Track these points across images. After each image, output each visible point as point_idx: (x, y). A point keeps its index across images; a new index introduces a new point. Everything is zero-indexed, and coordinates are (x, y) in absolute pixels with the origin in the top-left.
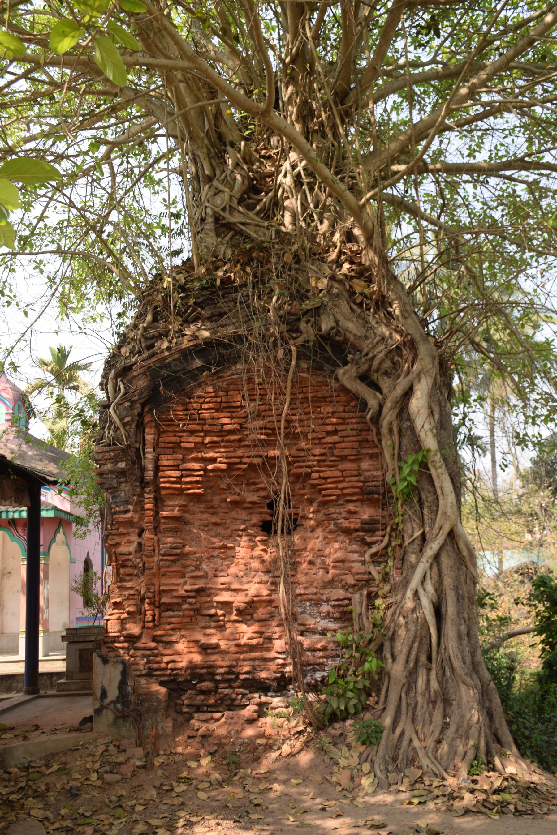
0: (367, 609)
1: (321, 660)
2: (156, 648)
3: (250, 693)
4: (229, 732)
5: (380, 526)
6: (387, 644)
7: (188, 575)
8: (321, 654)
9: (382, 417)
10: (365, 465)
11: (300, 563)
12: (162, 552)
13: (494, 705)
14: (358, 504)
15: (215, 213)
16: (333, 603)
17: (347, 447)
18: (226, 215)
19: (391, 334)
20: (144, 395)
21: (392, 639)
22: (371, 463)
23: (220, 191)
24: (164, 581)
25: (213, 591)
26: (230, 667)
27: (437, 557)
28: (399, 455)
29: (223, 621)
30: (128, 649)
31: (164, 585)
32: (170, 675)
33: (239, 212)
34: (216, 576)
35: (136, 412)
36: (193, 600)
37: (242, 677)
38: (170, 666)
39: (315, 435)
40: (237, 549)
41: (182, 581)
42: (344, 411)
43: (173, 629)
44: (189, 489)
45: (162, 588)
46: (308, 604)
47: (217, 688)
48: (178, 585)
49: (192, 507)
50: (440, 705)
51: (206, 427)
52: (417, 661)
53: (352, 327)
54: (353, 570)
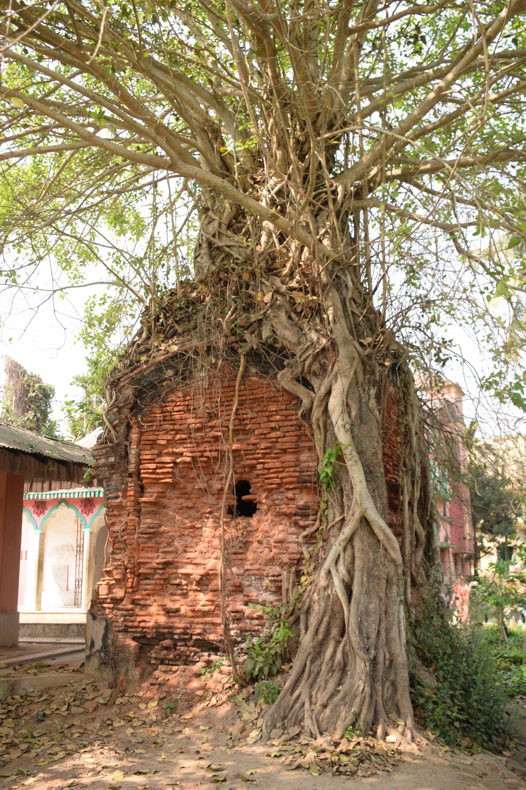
0: (294, 586)
1: (257, 628)
3: (202, 651)
4: (178, 683)
5: (310, 511)
6: (303, 617)
7: (160, 550)
8: (257, 622)
10: (304, 457)
11: (252, 542)
13: (399, 679)
14: (297, 491)
16: (271, 578)
17: (287, 442)
19: (318, 339)
21: (308, 612)
22: (309, 454)
24: (142, 555)
25: (179, 564)
26: (185, 628)
27: (350, 540)
29: (186, 589)
30: (113, 609)
32: (141, 632)
34: (185, 551)
36: (161, 571)
37: (194, 637)
38: (142, 624)
39: (261, 431)
40: (204, 529)
42: (286, 409)
43: (148, 595)
44: (163, 479)
46: (253, 578)
47: (175, 645)
48: (152, 558)
49: (168, 493)
50: (337, 675)
51: (176, 427)
53: (287, 335)
54: (290, 550)
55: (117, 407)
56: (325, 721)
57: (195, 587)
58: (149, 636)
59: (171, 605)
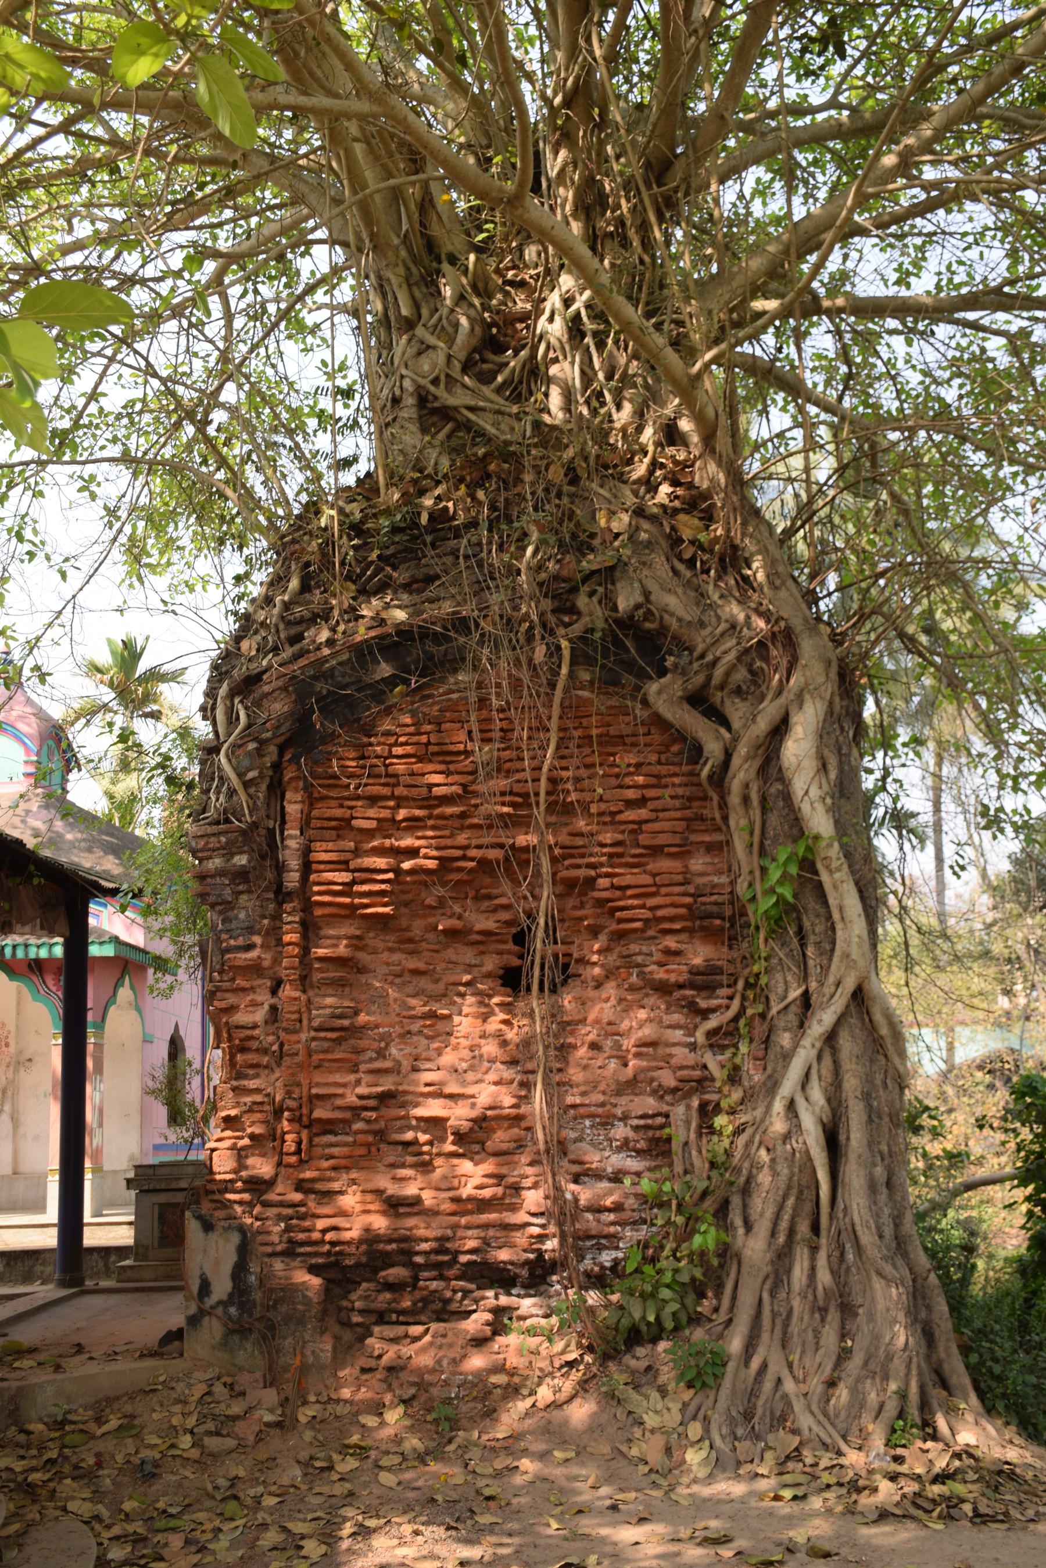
0: (700, 1135)
1: (612, 1229)
2: (302, 1204)
3: (479, 1288)
4: (439, 1362)
6: (736, 1201)
7: (363, 1067)
8: (612, 1217)
9: (730, 773)
10: (698, 863)
11: (575, 1047)
12: (316, 1023)
13: (935, 1317)
14: (684, 937)
15: (419, 387)
16: (635, 1122)
17: (664, 830)
18: (440, 392)
19: (748, 617)
20: (283, 729)
21: (746, 1191)
22: (708, 860)
23: (429, 347)
24: (318, 1078)
25: (409, 1098)
26: (442, 1239)
27: (831, 1038)
28: (762, 845)
29: (429, 1153)
30: (251, 1204)
31: (318, 1084)
32: (329, 1253)
33: (464, 386)
34: (416, 1070)
35: (268, 761)
36: (373, 1115)
37: (464, 1259)
38: (328, 1237)
39: (603, 806)
40: (457, 1019)
41: (352, 1077)
42: (659, 763)
43: (334, 1168)
44: (367, 906)
45: (314, 1091)
46: (587, 1123)
47: (416, 1279)
48: (344, 1085)
51: (399, 791)
52: (792, 1232)
53: (675, 604)
54: (674, 1061)
55: (256, 739)
56: (843, 1414)
57: (453, 1148)
58: (349, 1262)
59: (392, 1189)
